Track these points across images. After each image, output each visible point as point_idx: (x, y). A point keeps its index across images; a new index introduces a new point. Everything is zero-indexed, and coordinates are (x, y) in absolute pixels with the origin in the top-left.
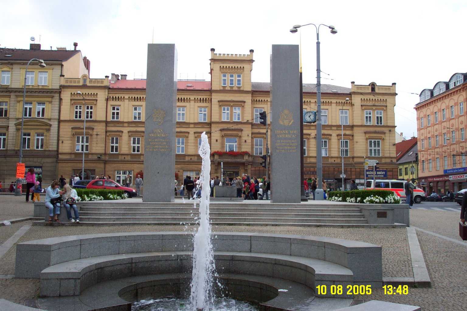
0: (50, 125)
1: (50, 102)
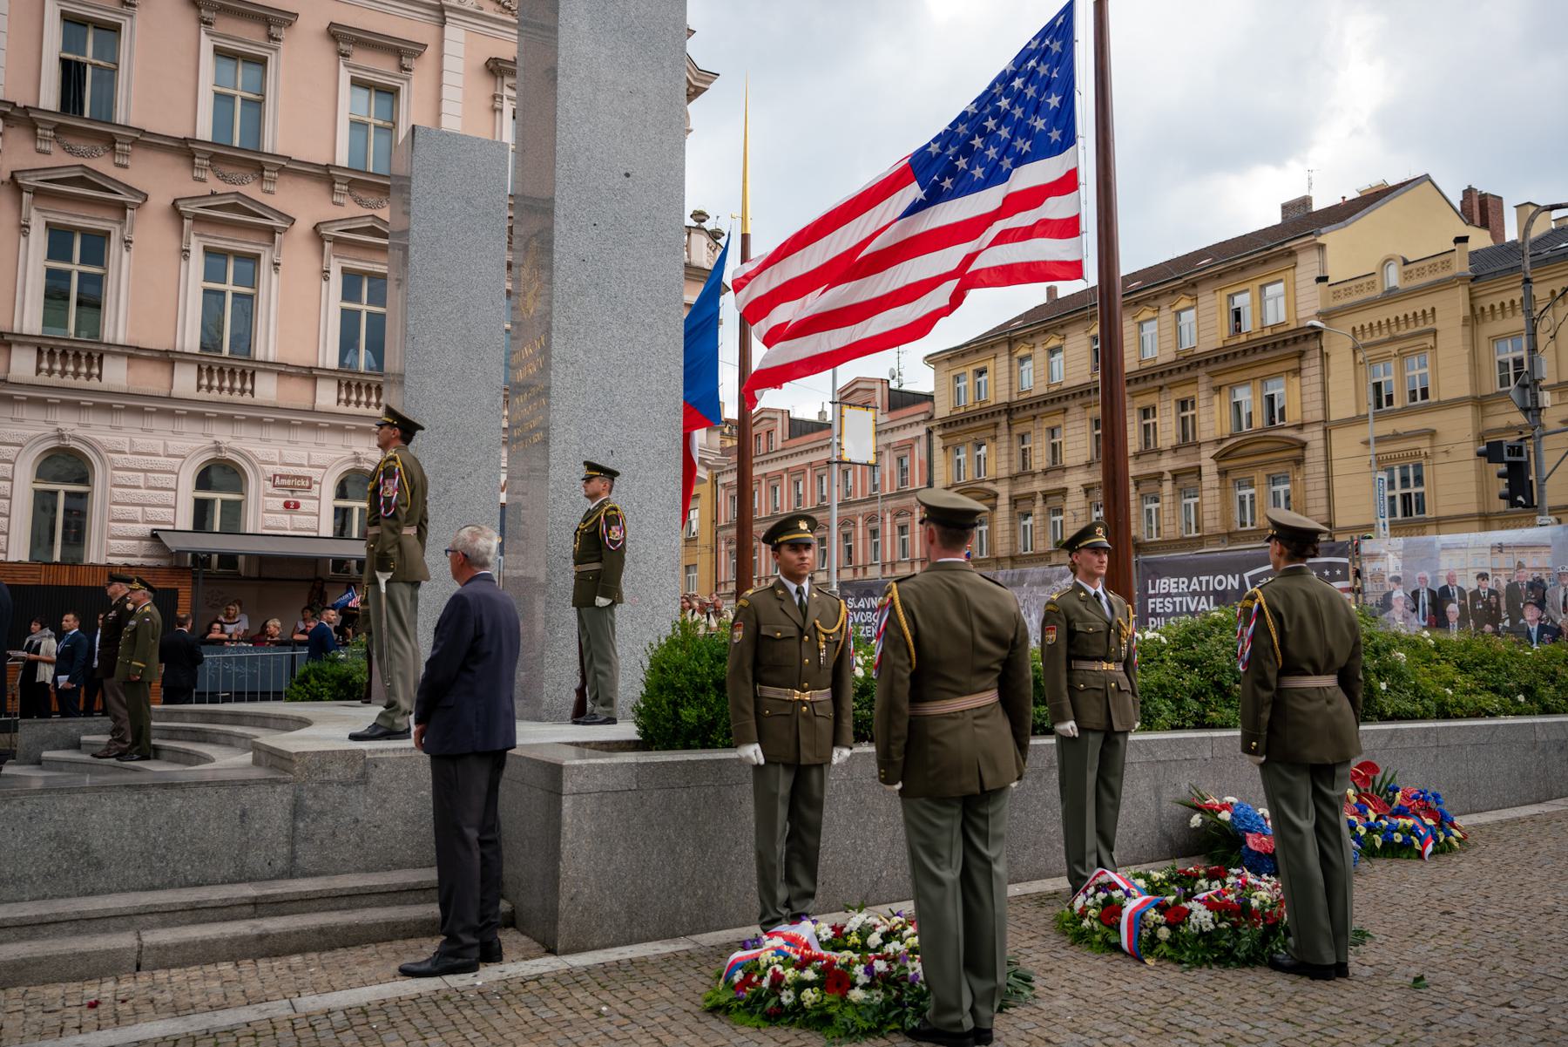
0: (1303, 445)
1: (1298, 372)
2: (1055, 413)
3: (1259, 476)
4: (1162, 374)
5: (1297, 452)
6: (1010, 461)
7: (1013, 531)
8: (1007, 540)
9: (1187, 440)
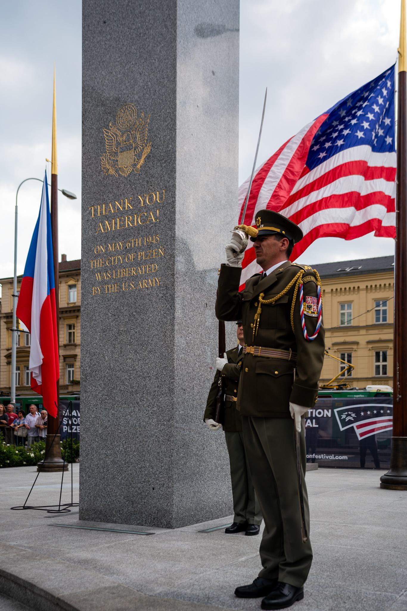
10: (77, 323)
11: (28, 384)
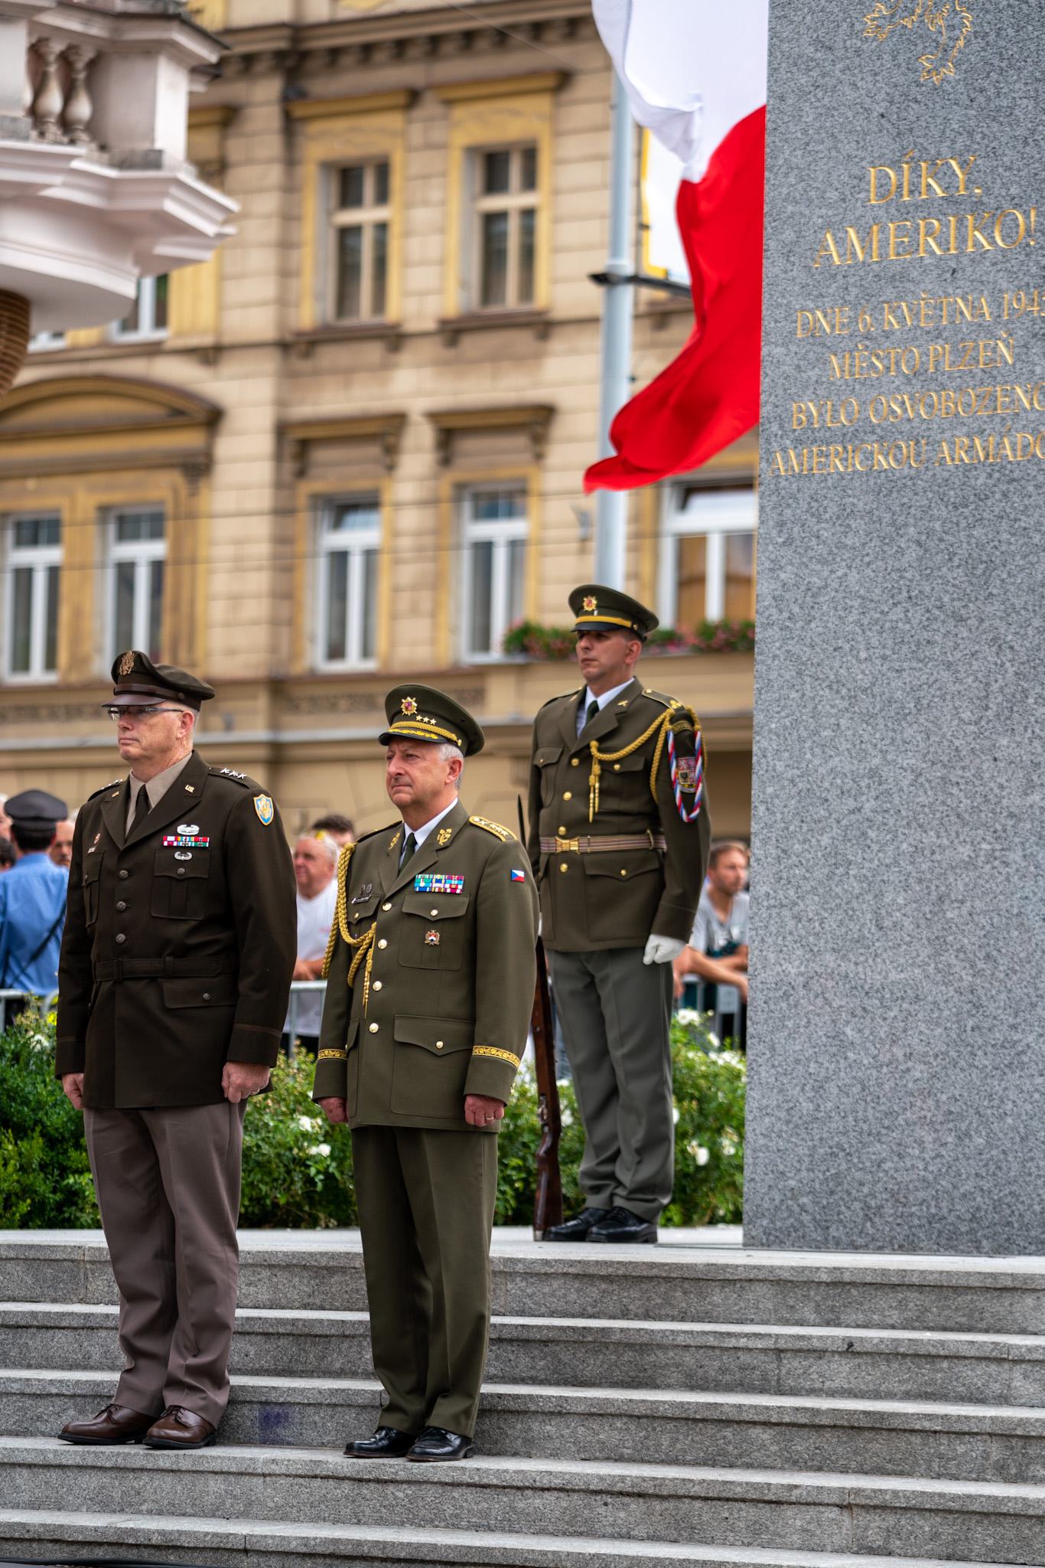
0: (213, 418)
2: (518, 85)
3: (78, 500)
4: (401, 47)
5: (189, 440)
6: (285, 273)
7: (285, 563)
8: (257, 608)
9: (500, 313)
10: (557, 134)
11: (336, 651)
